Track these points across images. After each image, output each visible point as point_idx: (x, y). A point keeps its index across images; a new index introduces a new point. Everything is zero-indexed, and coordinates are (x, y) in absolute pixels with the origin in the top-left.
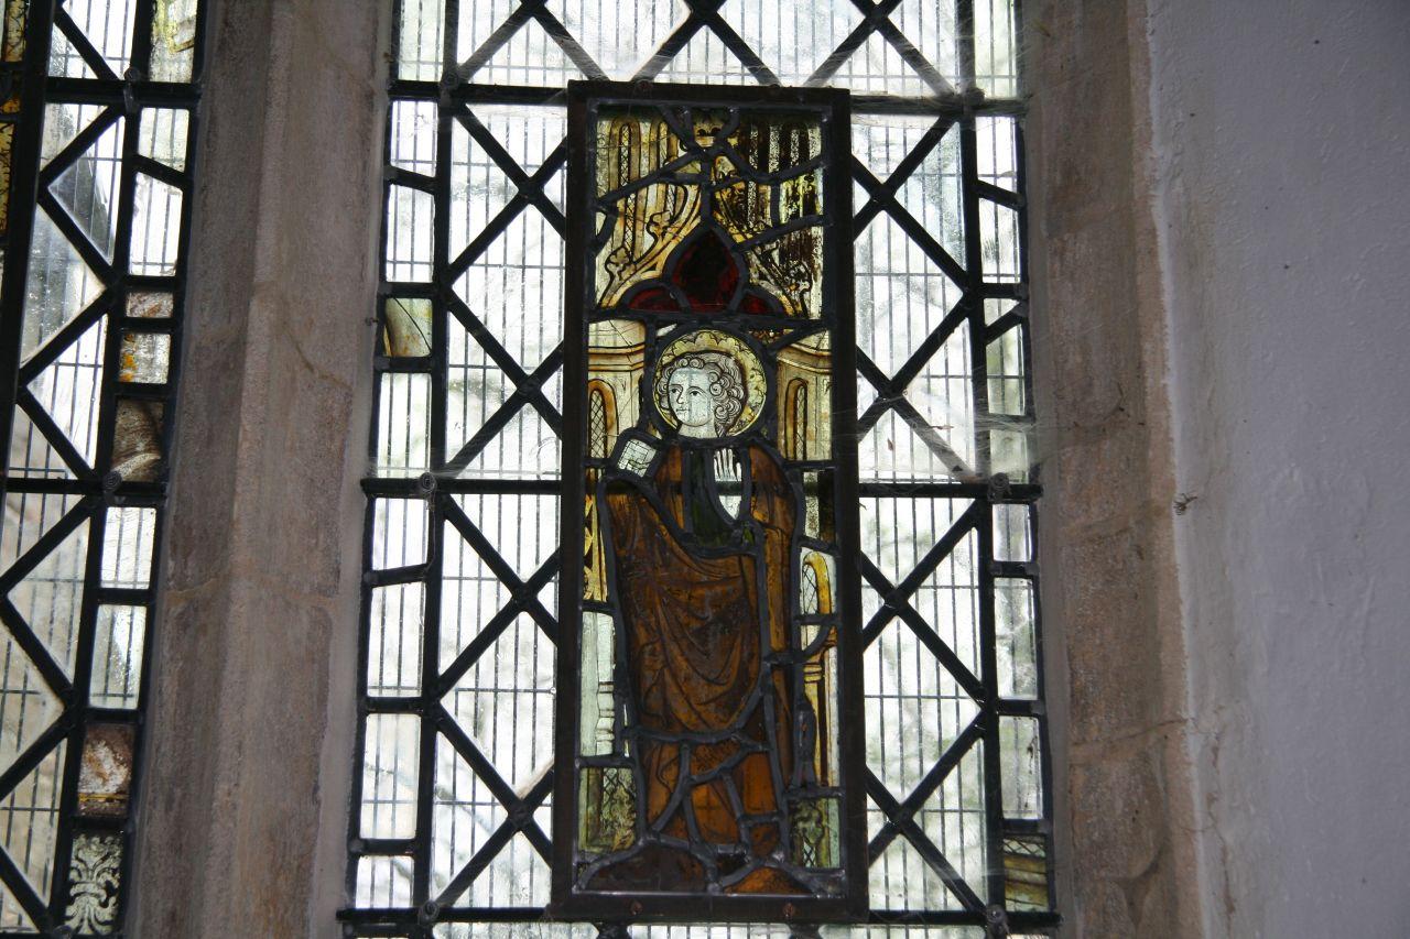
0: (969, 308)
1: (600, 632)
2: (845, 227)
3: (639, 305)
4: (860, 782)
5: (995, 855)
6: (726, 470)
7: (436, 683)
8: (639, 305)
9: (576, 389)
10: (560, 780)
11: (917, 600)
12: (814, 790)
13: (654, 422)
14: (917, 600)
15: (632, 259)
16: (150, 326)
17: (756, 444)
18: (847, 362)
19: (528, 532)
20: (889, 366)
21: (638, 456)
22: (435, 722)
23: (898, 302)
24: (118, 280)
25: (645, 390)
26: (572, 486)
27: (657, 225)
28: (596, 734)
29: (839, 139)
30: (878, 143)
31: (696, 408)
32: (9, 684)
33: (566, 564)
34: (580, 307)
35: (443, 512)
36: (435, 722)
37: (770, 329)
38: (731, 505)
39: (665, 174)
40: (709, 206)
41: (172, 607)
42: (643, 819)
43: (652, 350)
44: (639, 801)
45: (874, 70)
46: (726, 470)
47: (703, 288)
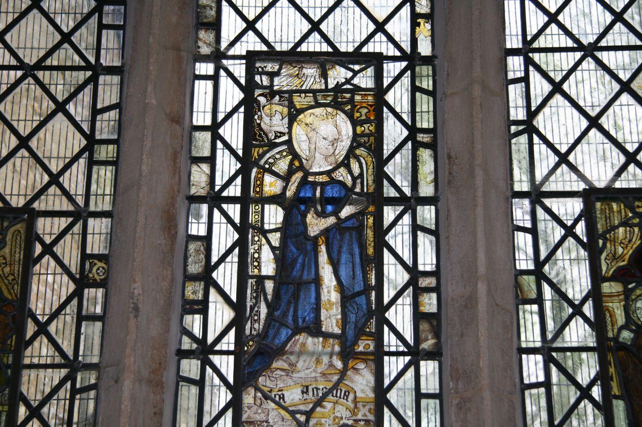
3: (619, 276)
8: (619, 276)
9: (599, 309)
15: (615, 257)
16: (428, 290)
25: (626, 309)
26: (604, 347)
33: (602, 377)
39: (625, 223)
43: (627, 293)
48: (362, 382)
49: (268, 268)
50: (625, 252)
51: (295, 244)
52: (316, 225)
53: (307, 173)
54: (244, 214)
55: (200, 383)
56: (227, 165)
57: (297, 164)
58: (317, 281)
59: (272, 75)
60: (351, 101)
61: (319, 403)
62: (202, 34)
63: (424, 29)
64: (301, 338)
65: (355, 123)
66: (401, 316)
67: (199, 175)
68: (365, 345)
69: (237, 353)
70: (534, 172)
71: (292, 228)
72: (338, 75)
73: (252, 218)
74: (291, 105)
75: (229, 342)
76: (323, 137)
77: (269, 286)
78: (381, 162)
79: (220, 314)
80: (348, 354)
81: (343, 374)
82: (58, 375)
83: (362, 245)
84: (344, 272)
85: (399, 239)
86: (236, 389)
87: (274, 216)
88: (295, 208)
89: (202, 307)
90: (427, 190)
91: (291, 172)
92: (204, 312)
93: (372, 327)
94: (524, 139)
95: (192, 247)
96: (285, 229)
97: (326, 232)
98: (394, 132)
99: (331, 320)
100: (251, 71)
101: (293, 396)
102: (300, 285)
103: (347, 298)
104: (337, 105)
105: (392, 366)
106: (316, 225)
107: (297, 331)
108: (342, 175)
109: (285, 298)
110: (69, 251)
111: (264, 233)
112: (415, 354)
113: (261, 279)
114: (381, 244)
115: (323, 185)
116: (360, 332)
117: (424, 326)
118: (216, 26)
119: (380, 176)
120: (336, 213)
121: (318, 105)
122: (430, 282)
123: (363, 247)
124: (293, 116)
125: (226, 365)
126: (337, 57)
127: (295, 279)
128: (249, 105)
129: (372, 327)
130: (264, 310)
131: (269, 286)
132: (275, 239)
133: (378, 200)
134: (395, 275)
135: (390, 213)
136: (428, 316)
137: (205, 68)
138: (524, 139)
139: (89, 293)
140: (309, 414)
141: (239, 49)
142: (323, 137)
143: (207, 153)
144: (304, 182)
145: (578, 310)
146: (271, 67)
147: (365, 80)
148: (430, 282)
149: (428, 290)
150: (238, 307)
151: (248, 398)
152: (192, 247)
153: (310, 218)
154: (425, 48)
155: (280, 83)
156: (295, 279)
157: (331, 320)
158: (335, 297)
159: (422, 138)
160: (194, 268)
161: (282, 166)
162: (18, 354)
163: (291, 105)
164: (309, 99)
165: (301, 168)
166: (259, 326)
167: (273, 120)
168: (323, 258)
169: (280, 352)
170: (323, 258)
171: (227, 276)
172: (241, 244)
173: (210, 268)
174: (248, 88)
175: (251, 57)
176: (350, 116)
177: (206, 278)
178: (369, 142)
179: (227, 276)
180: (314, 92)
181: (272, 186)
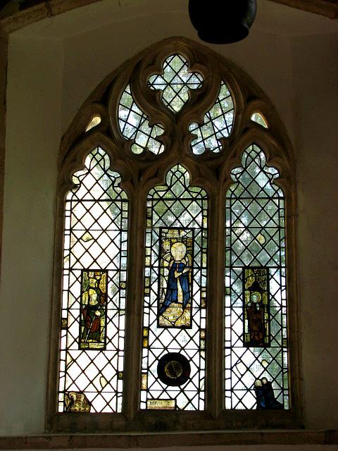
0: (280, 288)
1: (246, 321)
2: (269, 280)
3: (249, 289)
4: (270, 335)
5: (282, 341)
6: (258, 305)
7: (231, 326)
8: (249, 289)
9: (244, 297)
10: (244, 334)
11: (253, 406)
12: (266, 336)
13: (251, 301)
14: (253, 406)
15: (248, 284)
16: (204, 291)
17: (261, 303)
18: (269, 293)
19: (240, 311)
20: (273, 294)
21: (249, 305)
22: (231, 329)
23: (274, 287)
24: (201, 287)
25: (250, 297)
26: (244, 307)
27: (251, 281)
28: (246, 332)
29: (268, 271)
30: (111, 274)
31: (255, 299)
32: (187, 214)
33: (243, 314)
34: (244, 289)
35: (232, 309)
36: (231, 329)
37: (261, 291)
38: (258, 309)
39: (251, 276)
40: (256, 279)
41: (209, 230)
42: (251, 339)
43: (251, 293)
44: (250, 337)
45: (112, 267)
46: (258, 305)
47: (256, 288)
48: (187, 315)
49: (165, 285)
50: (251, 283)
51: (172, 280)
52: (177, 275)
53: (175, 261)
54: (159, 271)
55: (149, 314)
56: (154, 258)
57: (172, 258)
58: (177, 289)
59: (166, 233)
60: (186, 241)
61: (177, 320)
62: (148, 220)
63: (206, 219)
64: (173, 304)
65: (187, 247)
66: (197, 298)
67: (147, 260)
68: (189, 305)
69: (158, 307)
70: (235, 444)
71: (171, 275)
72: (183, 233)
73: (162, 273)
74: (171, 242)
75: (155, 304)
76: (178, 251)
77: (165, 290)
78: (193, 257)
79: (154, 297)
80: (184, 308)
81: (183, 313)
82: (116, 311)
83: (188, 280)
84: (184, 286)
85: (197, 278)
86: (158, 316)
87: (166, 272)
88: (172, 270)
89: (149, 295)
90: (204, 265)
91: (171, 260)
92: (149, 296)
93: (190, 302)
94: (229, 252)
95: (146, 279)
96: (169, 275)
97: (179, 277)
98: (197, 249)
99: (180, 299)
100: (161, 232)
101: (171, 318)
102: (172, 290)
103: (184, 294)
104: (182, 242)
105: (194, 311)
106: (177, 275)
107: (172, 302)
108: (183, 261)
109: (169, 294)
110: (116, 280)
111: (164, 276)
112: (200, 308)
113: (163, 289)
114: (193, 279)
115: (179, 264)
116: (187, 303)
117: (202, 301)
118: (151, 218)
119: (193, 261)
120: (182, 272)
121: (178, 242)
122: (205, 289)
123: (188, 281)
124: (171, 245)
125: (155, 310)
126: (184, 229)
127: (172, 289)
128: (160, 241)
129: (190, 302)
130: (164, 297)
131: (165, 290)
132: (167, 278)
133: (192, 268)
134: (196, 288)
135: (195, 271)
136: (204, 298)
137: (149, 230)
138: (229, 252)
139: (147, 326)
140: (175, 322)
141: (158, 225)
142: (178, 251)
143: (149, 254)
144: (174, 263)
145: (239, 297)
146: (166, 230)
147: (190, 236)
148: (205, 289)
149: (204, 291)
150: (158, 295)
151: (161, 318)
152: (146, 279)
153: (175, 273)
154: (205, 226)
155: (169, 236)
156: (172, 289)
157: (180, 299)
158: (181, 294)
159: (204, 250)
160: (147, 285)
161: (169, 259)
162: (106, 307)
163: (171, 242)
164: (176, 240)
165: (173, 259)
166: (163, 301)
167: (166, 246)
168: (179, 284)
169: (168, 307)
170: (179, 284)
171: (155, 287)
172: (159, 278)
173: (150, 285)
174: (160, 236)
175: (161, 228)
176: (186, 245)
177: (150, 287)
178: (190, 252)
179: (155, 287)
180: (176, 238)
181: (166, 264)
